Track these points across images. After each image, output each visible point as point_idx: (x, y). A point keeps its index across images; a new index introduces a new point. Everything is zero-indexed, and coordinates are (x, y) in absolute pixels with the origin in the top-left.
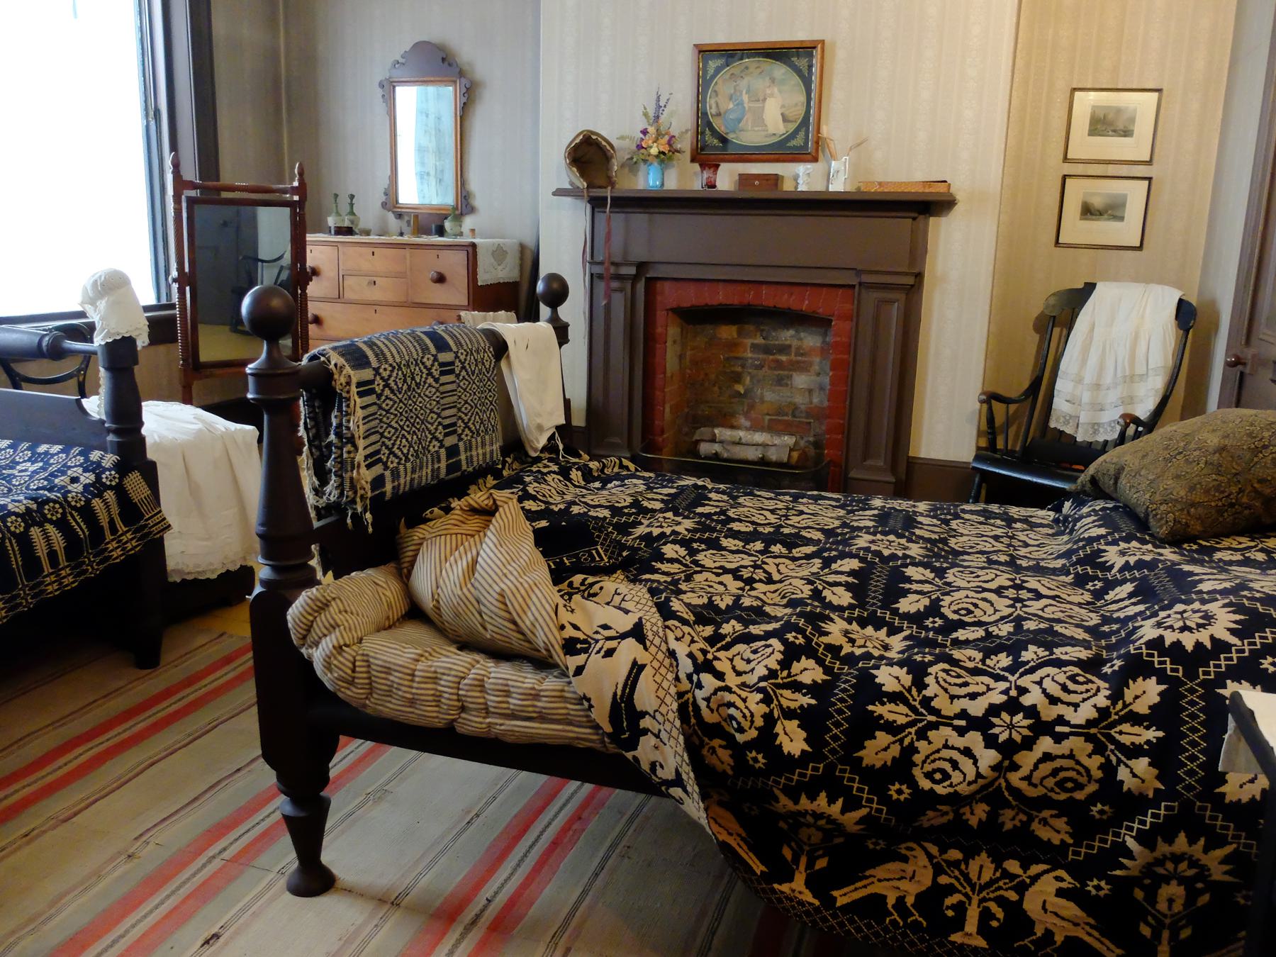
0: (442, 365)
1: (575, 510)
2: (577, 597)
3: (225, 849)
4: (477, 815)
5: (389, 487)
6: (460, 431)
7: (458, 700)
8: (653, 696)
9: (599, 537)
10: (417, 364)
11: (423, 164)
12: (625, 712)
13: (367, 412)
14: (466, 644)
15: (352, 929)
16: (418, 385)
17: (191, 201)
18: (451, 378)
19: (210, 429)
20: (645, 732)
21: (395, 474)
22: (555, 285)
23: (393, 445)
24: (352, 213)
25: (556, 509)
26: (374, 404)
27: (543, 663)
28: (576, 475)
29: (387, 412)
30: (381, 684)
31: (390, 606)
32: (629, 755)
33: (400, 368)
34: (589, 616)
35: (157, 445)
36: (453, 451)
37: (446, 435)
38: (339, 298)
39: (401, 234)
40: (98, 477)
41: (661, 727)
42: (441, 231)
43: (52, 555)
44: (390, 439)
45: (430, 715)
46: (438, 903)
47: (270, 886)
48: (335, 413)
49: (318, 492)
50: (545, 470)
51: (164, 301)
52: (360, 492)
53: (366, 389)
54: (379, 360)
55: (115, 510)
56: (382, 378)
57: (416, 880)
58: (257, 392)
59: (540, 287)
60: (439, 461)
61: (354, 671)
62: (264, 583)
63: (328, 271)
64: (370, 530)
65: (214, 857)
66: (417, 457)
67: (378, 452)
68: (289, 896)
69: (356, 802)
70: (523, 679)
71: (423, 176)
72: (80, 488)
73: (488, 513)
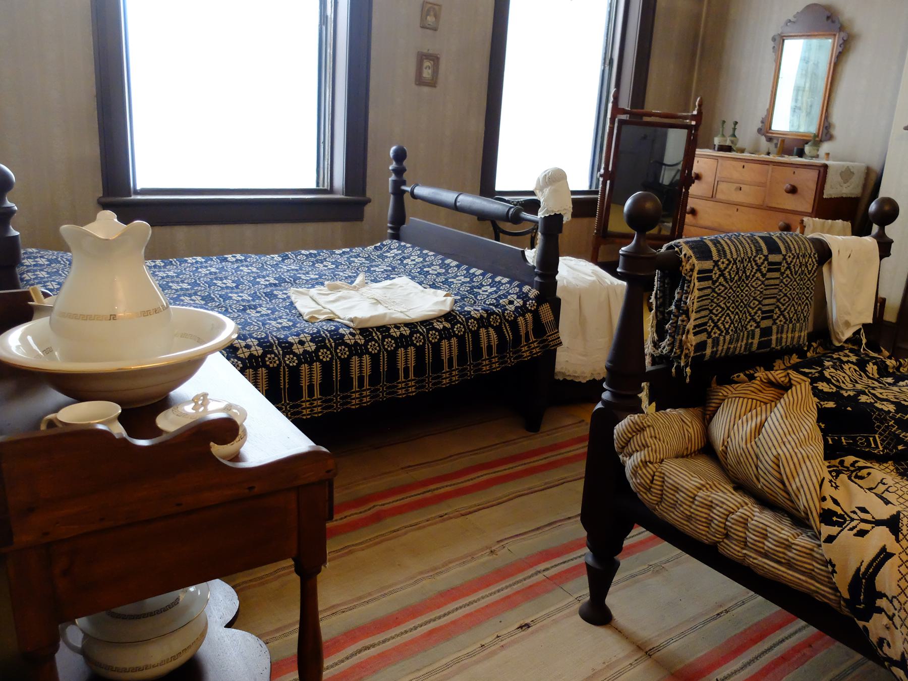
0: (770, 264)
1: (863, 399)
2: (844, 477)
3: (547, 569)
4: (727, 611)
5: (708, 351)
6: (775, 317)
7: (725, 529)
8: (894, 584)
9: (879, 427)
10: (749, 261)
11: (796, 100)
12: (865, 585)
13: (702, 293)
14: (742, 486)
15: (614, 659)
16: (747, 277)
17: (621, 122)
18: (777, 275)
19: (600, 280)
20: (880, 610)
21: (716, 342)
22: (887, 208)
23: (719, 320)
24: (734, 135)
25: (846, 395)
26: (709, 287)
27: (800, 522)
28: (871, 368)
29: (719, 295)
30: (669, 496)
31: (690, 440)
32: (861, 624)
33: (735, 263)
34: (850, 495)
35: (564, 288)
36: (766, 332)
37: (763, 318)
38: (712, 197)
39: (768, 154)
40: (525, 303)
41: (896, 612)
42: (801, 153)
43: (490, 347)
44: (716, 315)
45: (700, 531)
46: (679, 667)
47: (568, 606)
48: (678, 290)
49: (656, 345)
50: (845, 359)
51: (593, 189)
52: (685, 351)
53: (705, 276)
54: (719, 255)
55: (530, 327)
56: (719, 269)
57: (668, 644)
58: (624, 268)
59: (873, 207)
60: (753, 338)
61: (652, 482)
62: (605, 403)
63: (708, 177)
64: (688, 380)
65: (539, 572)
66: (736, 332)
67: (705, 324)
68: (578, 618)
69: (641, 568)
70: (783, 530)
71: (795, 109)
72: (513, 308)
73: (784, 388)
